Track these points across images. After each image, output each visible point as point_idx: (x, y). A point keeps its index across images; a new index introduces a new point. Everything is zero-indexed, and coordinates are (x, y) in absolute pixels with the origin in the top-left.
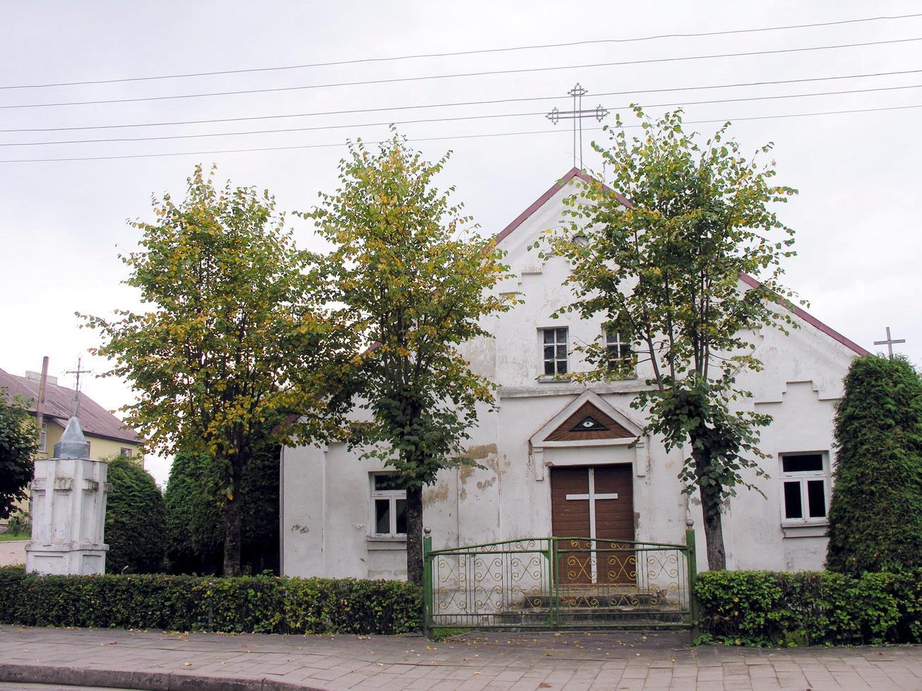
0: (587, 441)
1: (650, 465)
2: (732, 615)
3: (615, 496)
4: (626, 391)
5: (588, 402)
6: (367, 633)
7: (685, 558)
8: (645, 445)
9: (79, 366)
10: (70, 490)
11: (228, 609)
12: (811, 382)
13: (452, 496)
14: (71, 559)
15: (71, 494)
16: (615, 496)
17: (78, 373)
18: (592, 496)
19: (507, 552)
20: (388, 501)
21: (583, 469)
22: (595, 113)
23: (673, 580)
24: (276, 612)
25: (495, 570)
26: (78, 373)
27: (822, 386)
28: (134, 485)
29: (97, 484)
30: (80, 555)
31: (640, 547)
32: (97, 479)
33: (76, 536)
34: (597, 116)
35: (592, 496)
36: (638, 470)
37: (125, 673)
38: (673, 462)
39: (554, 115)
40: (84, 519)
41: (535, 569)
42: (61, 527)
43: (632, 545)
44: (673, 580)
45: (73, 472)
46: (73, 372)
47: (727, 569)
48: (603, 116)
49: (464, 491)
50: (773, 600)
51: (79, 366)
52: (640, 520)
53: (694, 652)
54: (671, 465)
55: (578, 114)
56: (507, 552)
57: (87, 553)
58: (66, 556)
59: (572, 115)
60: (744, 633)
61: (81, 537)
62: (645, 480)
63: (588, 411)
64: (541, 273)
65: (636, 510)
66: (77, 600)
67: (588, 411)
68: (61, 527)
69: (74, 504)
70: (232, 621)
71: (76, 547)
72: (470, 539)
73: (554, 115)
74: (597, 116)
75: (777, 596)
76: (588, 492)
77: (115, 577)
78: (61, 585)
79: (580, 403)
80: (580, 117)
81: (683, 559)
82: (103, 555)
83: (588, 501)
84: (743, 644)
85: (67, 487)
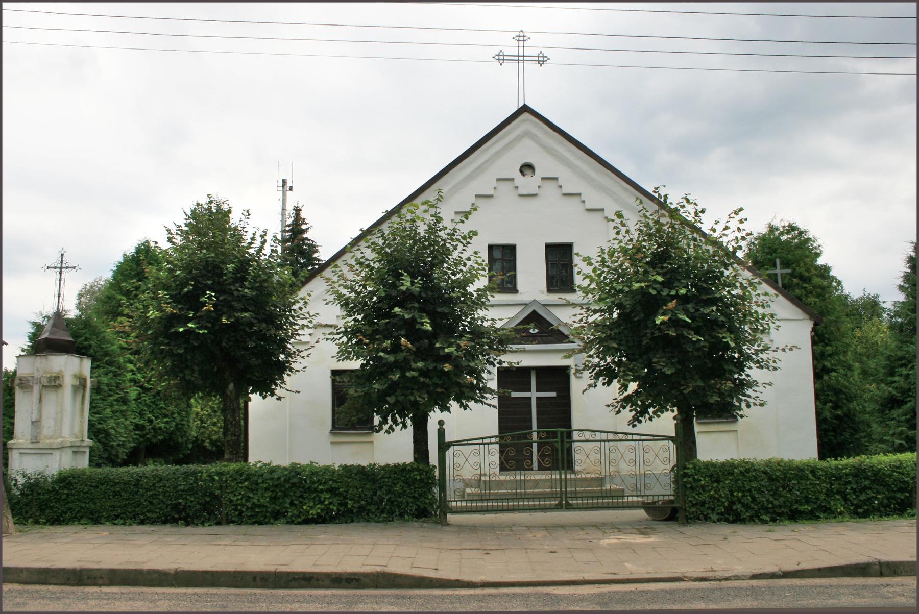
3: (553, 394)
5: (534, 312)
9: (62, 262)
14: (61, 456)
16: (553, 394)
17: (61, 268)
19: (605, 441)
21: (527, 370)
23: (665, 467)
25: (594, 457)
26: (61, 268)
30: (70, 451)
31: (493, 440)
34: (539, 61)
35: (534, 394)
37: (652, 591)
39: (501, 58)
41: (663, 455)
43: (569, 435)
46: (55, 268)
51: (62, 262)
55: (521, 59)
56: (605, 441)
57: (76, 449)
63: (534, 318)
64: (491, 196)
67: (534, 318)
69: (83, 397)
73: (501, 58)
74: (539, 61)
76: (538, 390)
77: (823, 464)
79: (528, 312)
82: (87, 450)
83: (530, 398)
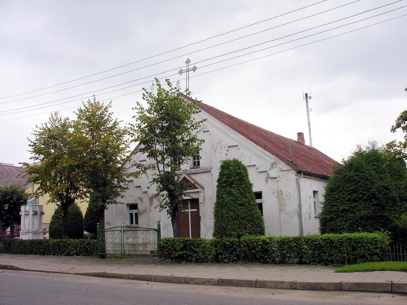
0: (192, 190)
1: (204, 199)
2: (294, 252)
4: (196, 172)
6: (87, 256)
7: (156, 233)
8: (202, 192)
10: (28, 215)
11: (56, 249)
12: (255, 165)
13: (148, 211)
15: (28, 216)
18: (190, 210)
20: (133, 213)
22: (183, 72)
24: (96, 251)
27: (259, 167)
28: (70, 211)
29: (37, 212)
31: (106, 230)
32: (37, 211)
33: (31, 228)
36: (200, 201)
38: (211, 198)
40: (33, 223)
42: (27, 226)
44: (142, 241)
45: (29, 209)
47: (202, 236)
48: (180, 71)
49: (150, 209)
50: (180, 248)
52: (201, 219)
53: (200, 263)
54: (210, 199)
58: (28, 234)
59: (189, 70)
60: (172, 258)
61: (33, 228)
62: (203, 204)
65: (200, 215)
66: (25, 247)
68: (27, 226)
70: (58, 252)
71: (30, 231)
72: (153, 226)
75: (181, 246)
78: (22, 243)
80: (188, 71)
81: (156, 233)
84: (88, 264)
85: (27, 214)
